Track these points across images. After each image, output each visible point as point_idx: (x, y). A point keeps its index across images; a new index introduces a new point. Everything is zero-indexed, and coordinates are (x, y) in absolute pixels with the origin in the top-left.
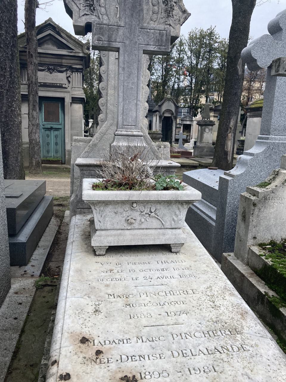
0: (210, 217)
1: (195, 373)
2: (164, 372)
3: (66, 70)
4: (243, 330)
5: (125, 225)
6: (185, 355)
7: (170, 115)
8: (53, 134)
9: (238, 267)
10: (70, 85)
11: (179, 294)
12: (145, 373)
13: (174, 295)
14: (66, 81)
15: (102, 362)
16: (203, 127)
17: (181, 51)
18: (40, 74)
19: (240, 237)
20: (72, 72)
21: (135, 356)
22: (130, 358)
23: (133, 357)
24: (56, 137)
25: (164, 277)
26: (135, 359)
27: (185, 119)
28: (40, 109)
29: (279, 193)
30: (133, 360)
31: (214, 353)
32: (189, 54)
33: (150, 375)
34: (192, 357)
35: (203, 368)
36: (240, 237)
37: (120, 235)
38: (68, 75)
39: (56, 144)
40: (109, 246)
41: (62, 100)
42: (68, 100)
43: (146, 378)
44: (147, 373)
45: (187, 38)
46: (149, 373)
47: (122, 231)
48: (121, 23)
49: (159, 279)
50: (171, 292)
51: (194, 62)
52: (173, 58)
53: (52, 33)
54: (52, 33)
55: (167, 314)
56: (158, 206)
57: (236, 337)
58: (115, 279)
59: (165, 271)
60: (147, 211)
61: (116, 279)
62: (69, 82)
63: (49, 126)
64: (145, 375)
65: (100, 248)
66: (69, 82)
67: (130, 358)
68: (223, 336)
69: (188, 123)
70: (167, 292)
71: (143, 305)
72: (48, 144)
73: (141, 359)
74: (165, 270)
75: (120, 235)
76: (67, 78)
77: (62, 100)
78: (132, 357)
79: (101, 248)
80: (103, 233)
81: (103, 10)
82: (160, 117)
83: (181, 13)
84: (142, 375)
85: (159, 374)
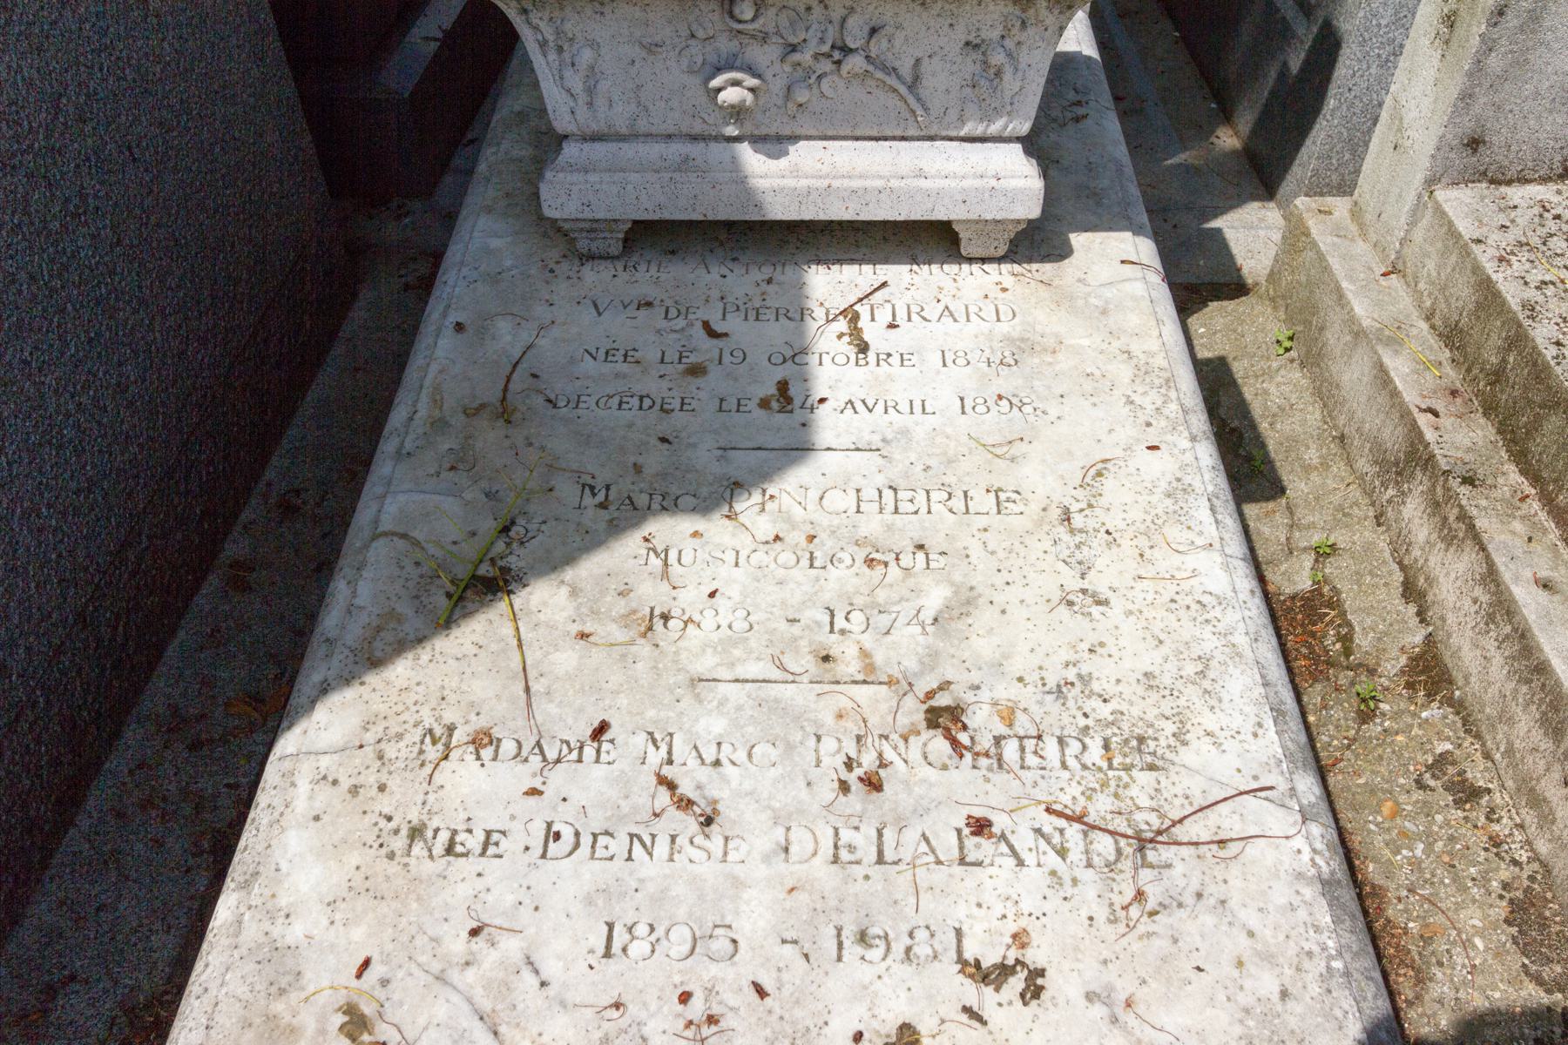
1: (863, 958)
2: (719, 931)
4: (1182, 749)
6: (844, 855)
11: (924, 510)
12: (630, 930)
13: (896, 511)
15: (459, 849)
19: (1399, 130)
21: (611, 835)
22: (586, 840)
23: (602, 840)
25: (880, 407)
26: (606, 848)
30: (600, 852)
31: (987, 861)
33: (653, 938)
34: (877, 872)
35: (911, 935)
36: (1399, 130)
37: (685, 164)
40: (635, 222)
43: (626, 955)
44: (642, 930)
46: (652, 929)
47: (695, 150)
48: (1485, 436)
49: (849, 411)
50: (888, 494)
55: (827, 619)
57: (1126, 786)
58: (635, 402)
59: (896, 369)
61: (641, 398)
64: (628, 937)
65: (594, 227)
67: (586, 840)
68: (1066, 775)
70: (869, 493)
71: (730, 557)
73: (637, 848)
74: (895, 360)
75: (685, 164)
78: (595, 836)
79: (595, 225)
80: (599, 150)
84: (615, 934)
85: (695, 940)
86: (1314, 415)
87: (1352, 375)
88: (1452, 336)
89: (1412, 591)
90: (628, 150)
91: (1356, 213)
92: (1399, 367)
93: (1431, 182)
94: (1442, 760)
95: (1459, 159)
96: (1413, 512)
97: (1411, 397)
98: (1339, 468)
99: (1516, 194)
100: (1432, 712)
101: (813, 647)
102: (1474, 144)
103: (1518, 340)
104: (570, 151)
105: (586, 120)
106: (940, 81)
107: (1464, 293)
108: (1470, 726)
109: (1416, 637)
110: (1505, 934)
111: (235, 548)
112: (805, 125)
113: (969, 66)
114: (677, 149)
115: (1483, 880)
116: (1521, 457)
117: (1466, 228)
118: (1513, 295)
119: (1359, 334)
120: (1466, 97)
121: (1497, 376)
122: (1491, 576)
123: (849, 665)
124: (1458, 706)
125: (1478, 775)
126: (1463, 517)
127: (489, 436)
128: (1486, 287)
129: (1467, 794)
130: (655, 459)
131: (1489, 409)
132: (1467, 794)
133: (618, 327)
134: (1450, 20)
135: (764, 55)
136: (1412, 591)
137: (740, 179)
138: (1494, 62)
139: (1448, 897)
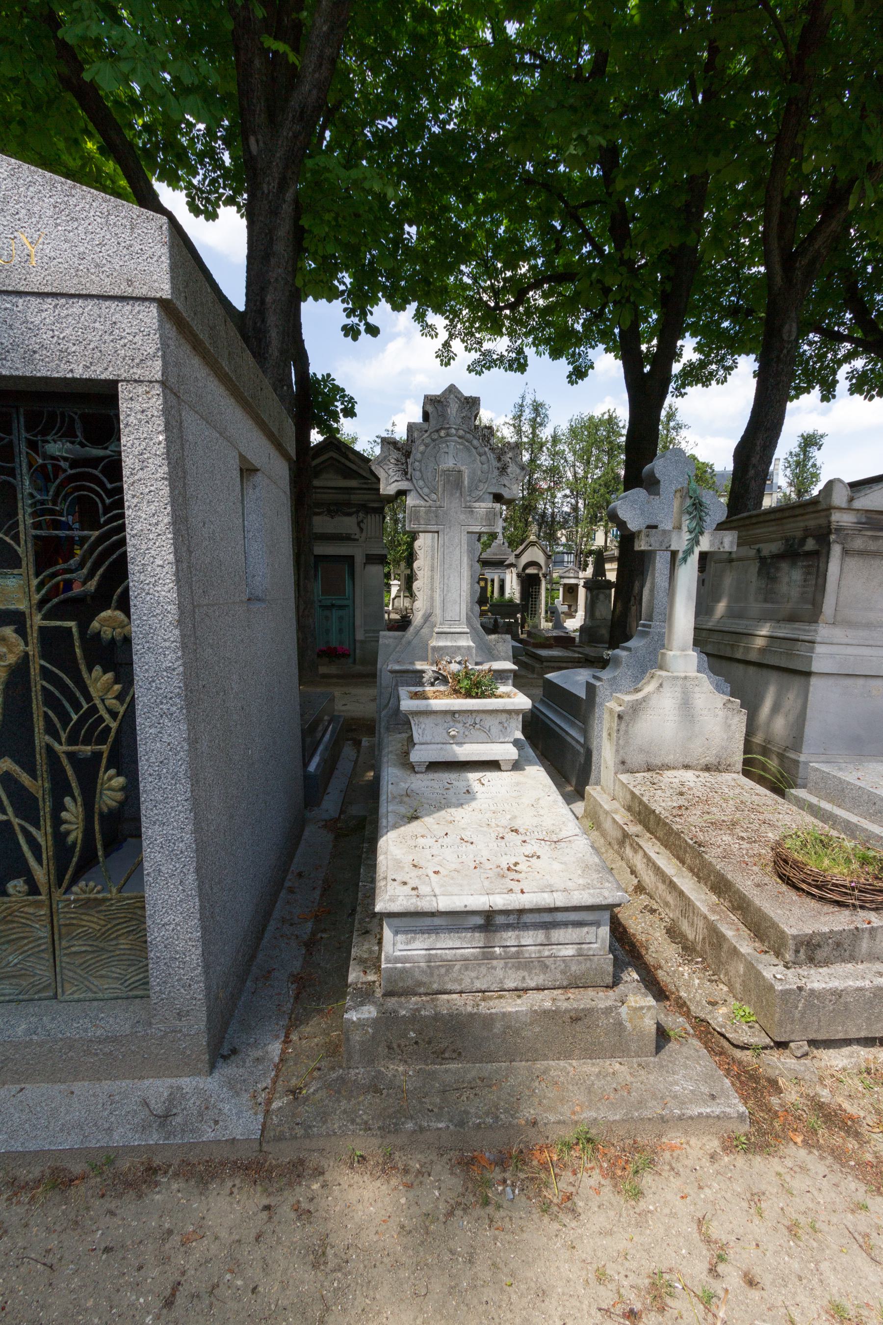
0: (577, 741)
3: (357, 512)
5: (448, 738)
7: (535, 572)
8: (335, 614)
9: (772, 915)
10: (364, 535)
14: (356, 530)
16: (595, 592)
17: (557, 453)
18: (317, 520)
20: (367, 513)
24: (341, 618)
27: (567, 575)
28: (316, 576)
29: (654, 701)
32: (570, 457)
38: (360, 519)
39: (341, 631)
41: (350, 559)
42: (359, 560)
45: (566, 431)
51: (580, 472)
52: (540, 466)
53: (335, 455)
54: (335, 455)
56: (483, 716)
60: (470, 721)
62: (361, 530)
63: (328, 603)
65: (420, 763)
66: (361, 530)
69: (573, 581)
72: (327, 631)
76: (359, 524)
77: (350, 559)
81: (418, 474)
82: (519, 576)
83: (518, 471)
86: (602, 841)
87: (608, 825)
88: (629, 809)
89: (633, 872)
90: (430, 747)
91: (602, 789)
92: (618, 818)
93: (616, 773)
94: (646, 906)
95: (621, 767)
96: (629, 852)
97: (621, 822)
98: (611, 851)
99: (637, 775)
100: (643, 897)
101: (533, 631)
102: (623, 763)
103: (641, 802)
104: (417, 747)
105: (423, 740)
106: (495, 730)
107: (629, 796)
108: (651, 897)
109: (635, 882)
110: (666, 936)
111: (287, 884)
112: (467, 740)
113: (500, 727)
114: (440, 746)
115: (659, 927)
116: (649, 831)
117: (625, 782)
118: (637, 792)
119: (607, 813)
120: (617, 751)
121: (639, 813)
122: (645, 855)
123: (493, 824)
124: (648, 894)
125: (655, 907)
126: (638, 844)
127: (406, 799)
128: (632, 793)
129: (653, 911)
130: (443, 801)
131: (640, 822)
132: (653, 911)
133: (429, 783)
134: (609, 735)
135: (458, 725)
136: (633, 872)
137: (454, 751)
138: (621, 742)
139: (651, 931)
